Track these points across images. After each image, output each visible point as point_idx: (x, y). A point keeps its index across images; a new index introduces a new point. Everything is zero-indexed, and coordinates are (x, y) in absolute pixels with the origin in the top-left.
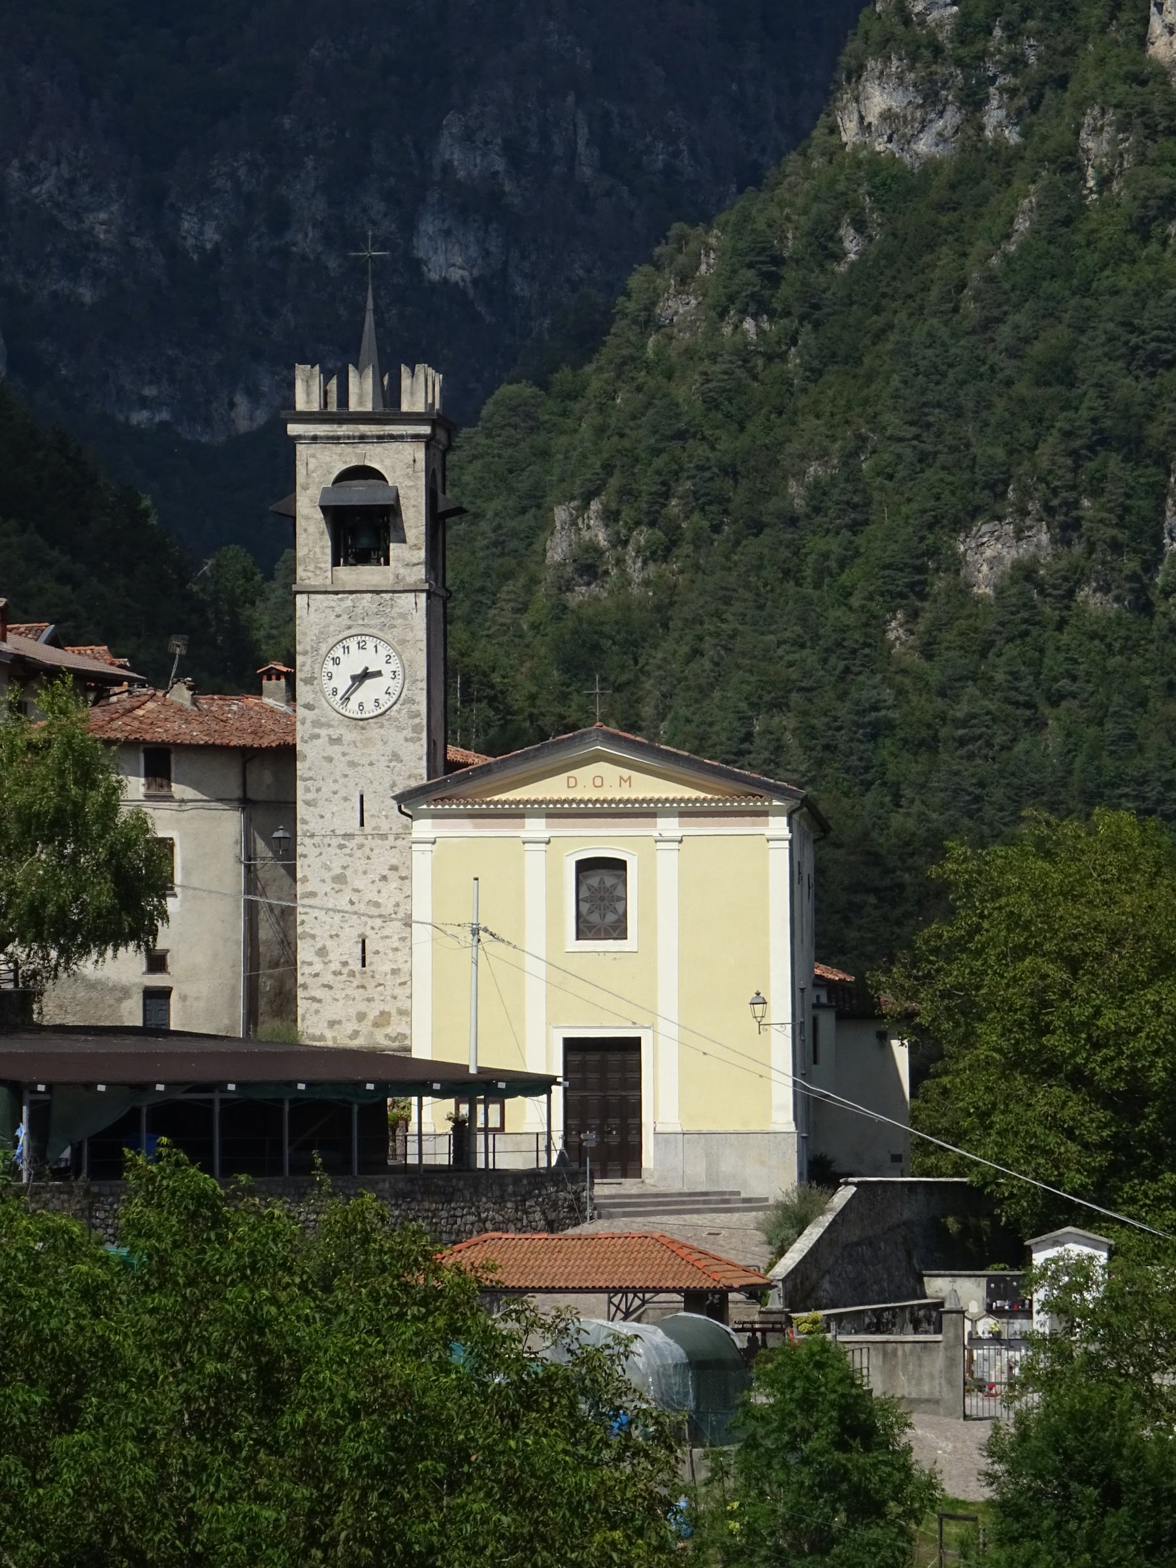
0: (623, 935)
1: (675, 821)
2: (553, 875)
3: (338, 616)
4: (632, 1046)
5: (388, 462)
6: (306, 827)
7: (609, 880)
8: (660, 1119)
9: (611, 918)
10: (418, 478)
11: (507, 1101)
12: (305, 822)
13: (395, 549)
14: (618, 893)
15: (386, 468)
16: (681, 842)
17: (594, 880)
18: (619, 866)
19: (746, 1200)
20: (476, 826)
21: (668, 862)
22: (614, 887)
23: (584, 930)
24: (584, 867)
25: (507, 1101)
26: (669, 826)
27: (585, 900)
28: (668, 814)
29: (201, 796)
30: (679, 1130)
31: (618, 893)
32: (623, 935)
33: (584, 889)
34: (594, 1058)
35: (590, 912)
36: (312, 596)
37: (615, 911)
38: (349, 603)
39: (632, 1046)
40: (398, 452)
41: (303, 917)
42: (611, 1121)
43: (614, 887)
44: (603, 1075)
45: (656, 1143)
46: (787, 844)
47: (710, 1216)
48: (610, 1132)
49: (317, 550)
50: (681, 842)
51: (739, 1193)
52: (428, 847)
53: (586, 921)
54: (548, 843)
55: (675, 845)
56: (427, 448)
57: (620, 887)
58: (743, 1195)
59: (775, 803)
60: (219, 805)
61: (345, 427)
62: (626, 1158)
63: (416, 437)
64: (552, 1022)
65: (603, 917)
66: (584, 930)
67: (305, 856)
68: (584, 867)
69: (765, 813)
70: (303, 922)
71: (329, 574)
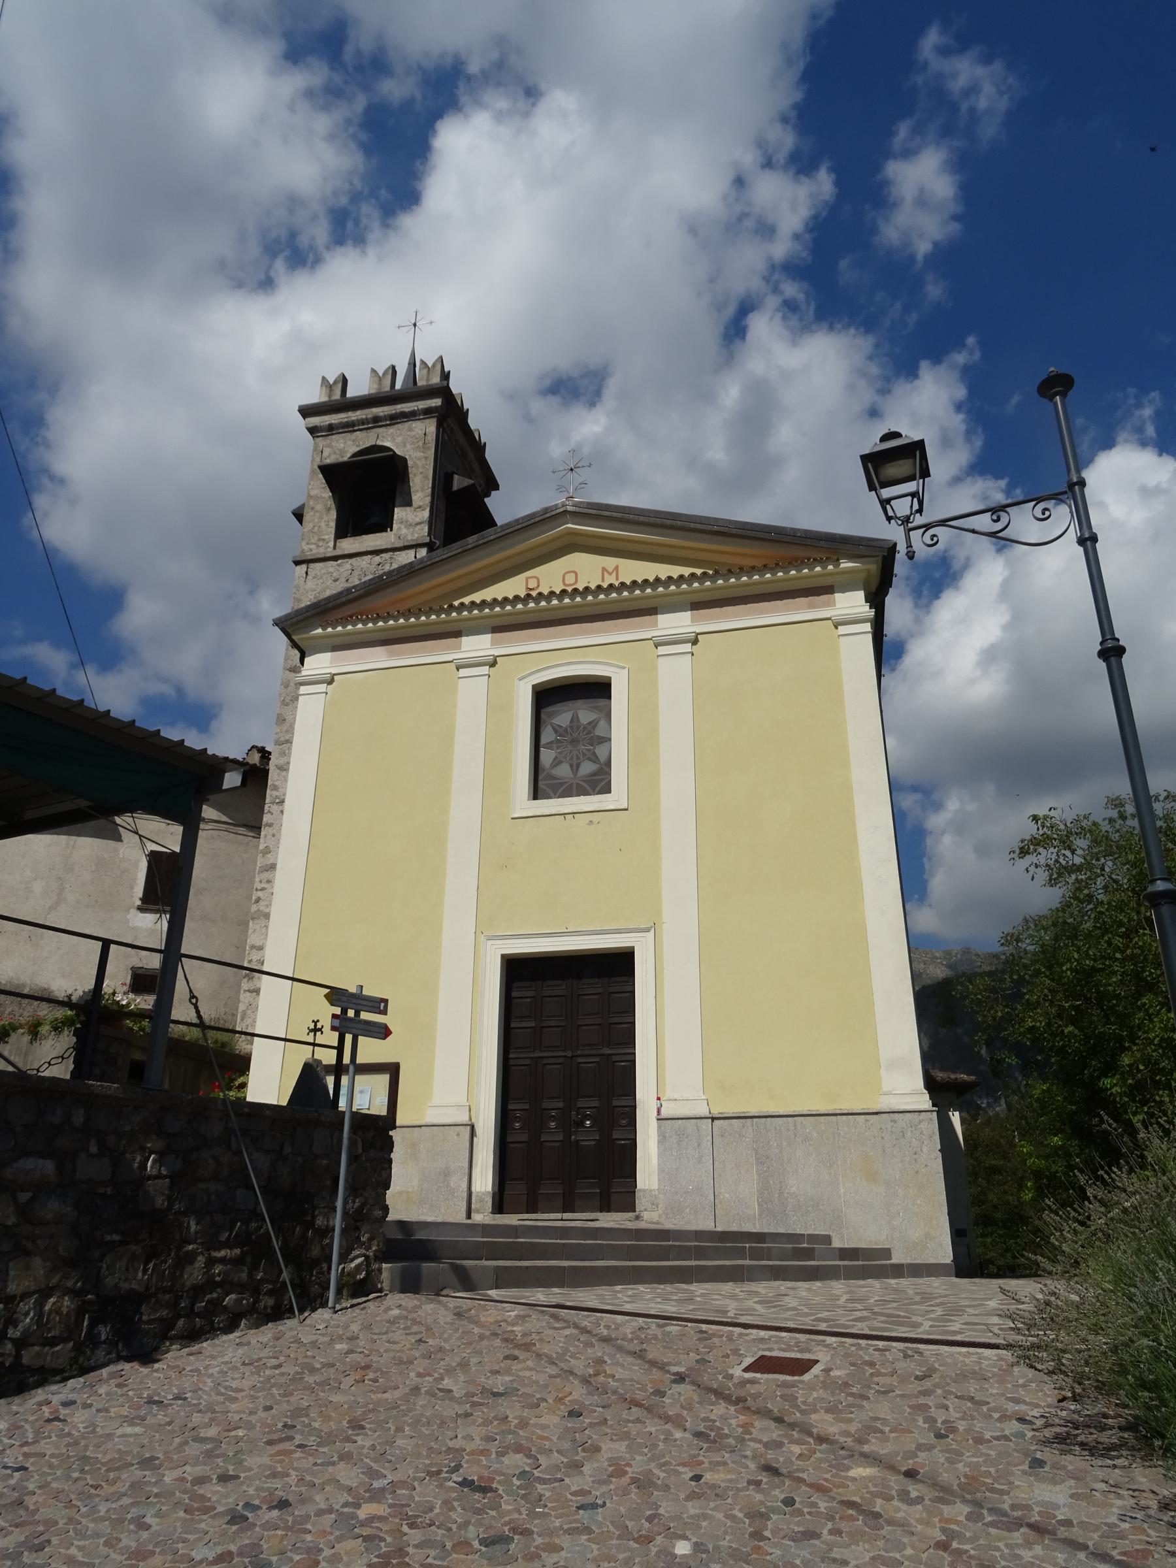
0: (607, 789)
1: (687, 615)
2: (497, 709)
3: (336, 580)
4: (620, 964)
5: (399, 439)
6: (275, 793)
7: (584, 712)
8: (669, 1093)
9: (587, 768)
10: (429, 448)
11: (183, 951)
12: (276, 788)
13: (399, 513)
14: (599, 732)
15: (397, 445)
16: (695, 642)
17: (562, 716)
18: (596, 690)
19: (845, 1253)
20: (391, 655)
21: (675, 673)
22: (593, 724)
23: (607, 974)
24: (548, 697)
25: (183, 951)
26: (678, 623)
27: (549, 746)
28: (674, 607)
29: (225, 819)
30: (703, 1110)
31: (599, 732)
32: (607, 789)
33: (547, 736)
34: (555, 989)
35: (557, 762)
36: (312, 565)
37: (594, 759)
38: (348, 566)
39: (620, 964)
40: (410, 429)
41: (260, 894)
42: (581, 1103)
43: (593, 724)
44: (568, 1020)
45: (662, 1138)
46: (867, 627)
47: (764, 1288)
48: (581, 1124)
49: (323, 524)
50: (695, 642)
51: (827, 1239)
52: (322, 687)
53: (551, 777)
54: (493, 664)
55: (687, 647)
56: (439, 425)
57: (602, 723)
58: (837, 1244)
59: (845, 565)
60: (241, 830)
61: (358, 413)
62: (606, 1168)
63: (428, 412)
64: (484, 930)
65: (575, 768)
66: (607, 974)
67: (270, 825)
68: (548, 697)
69: (826, 590)
70: (258, 900)
71: (331, 544)
